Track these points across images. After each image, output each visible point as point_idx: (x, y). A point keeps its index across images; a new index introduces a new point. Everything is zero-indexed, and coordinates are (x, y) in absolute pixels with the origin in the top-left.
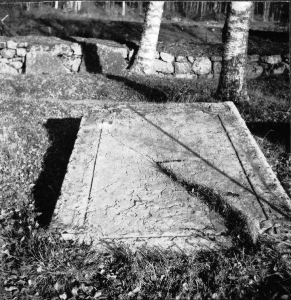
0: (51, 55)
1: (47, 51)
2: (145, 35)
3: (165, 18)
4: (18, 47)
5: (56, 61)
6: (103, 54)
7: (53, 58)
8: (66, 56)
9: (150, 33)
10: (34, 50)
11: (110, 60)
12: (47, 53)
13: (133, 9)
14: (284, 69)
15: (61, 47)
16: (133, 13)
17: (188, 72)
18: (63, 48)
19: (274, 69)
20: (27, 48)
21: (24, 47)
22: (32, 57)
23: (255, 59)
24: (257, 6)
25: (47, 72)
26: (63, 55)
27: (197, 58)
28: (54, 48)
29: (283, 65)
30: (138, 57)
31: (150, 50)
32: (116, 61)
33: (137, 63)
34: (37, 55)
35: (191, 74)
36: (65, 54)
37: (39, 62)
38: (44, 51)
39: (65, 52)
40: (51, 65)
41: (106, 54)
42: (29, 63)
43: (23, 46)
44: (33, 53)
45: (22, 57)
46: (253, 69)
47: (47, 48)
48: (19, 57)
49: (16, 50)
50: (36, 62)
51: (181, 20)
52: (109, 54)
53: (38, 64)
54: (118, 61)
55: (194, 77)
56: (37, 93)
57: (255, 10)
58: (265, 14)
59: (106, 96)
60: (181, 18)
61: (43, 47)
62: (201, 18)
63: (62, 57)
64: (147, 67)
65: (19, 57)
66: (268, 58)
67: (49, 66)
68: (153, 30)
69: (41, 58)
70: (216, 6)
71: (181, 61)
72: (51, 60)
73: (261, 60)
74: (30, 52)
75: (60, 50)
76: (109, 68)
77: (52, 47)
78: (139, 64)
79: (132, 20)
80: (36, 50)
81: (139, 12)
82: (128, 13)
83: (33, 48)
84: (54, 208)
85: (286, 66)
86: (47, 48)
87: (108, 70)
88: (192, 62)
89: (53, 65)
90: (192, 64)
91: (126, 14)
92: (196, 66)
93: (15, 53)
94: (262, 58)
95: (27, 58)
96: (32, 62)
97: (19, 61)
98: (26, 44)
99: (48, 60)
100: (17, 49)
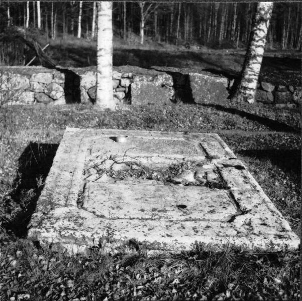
0: (155, 85)
1: (151, 81)
2: (249, 65)
4: (122, 78)
5: (160, 91)
6: (205, 84)
7: (157, 89)
8: (168, 87)
9: (254, 63)
10: (138, 80)
11: (212, 90)
12: (150, 83)
13: (150, 38)
15: (164, 77)
16: (151, 41)
17: (289, 101)
18: (165, 78)
20: (131, 79)
21: (128, 78)
22: (137, 87)
24: (94, 24)
25: (152, 102)
27: (297, 87)
28: (158, 79)
30: (240, 87)
31: (254, 80)
32: (218, 91)
33: (240, 92)
34: (142, 86)
35: (291, 103)
36: (167, 85)
37: (144, 92)
38: (147, 81)
39: (167, 82)
40: (156, 94)
41: (209, 84)
42: (134, 93)
43: (127, 76)
44: (137, 83)
45: (125, 87)
47: (151, 78)
48: (123, 87)
49: (120, 81)
50: (141, 92)
51: (200, 49)
52: (211, 84)
53: (143, 95)
54: (220, 91)
55: (294, 106)
56: (166, 124)
57: (136, 34)
58: (284, 42)
59: (234, 126)
60: (200, 47)
61: (146, 77)
62: (220, 46)
63: (165, 87)
64: (251, 97)
65: (123, 87)
67: (154, 96)
68: (257, 60)
69: (146, 88)
71: (282, 90)
72: (156, 91)
74: (135, 83)
75: (162, 80)
76: (211, 98)
77: (155, 77)
78: (242, 94)
79: (153, 48)
80: (140, 81)
81: (157, 40)
82: (146, 41)
83: (137, 79)
86: (151, 78)
87: (210, 100)
88: (292, 91)
89: (158, 95)
90: (292, 93)
91: (144, 42)
93: (118, 84)
95: (132, 89)
96: (137, 92)
97: (122, 91)
98: (130, 75)
99: (152, 90)
100: (122, 80)
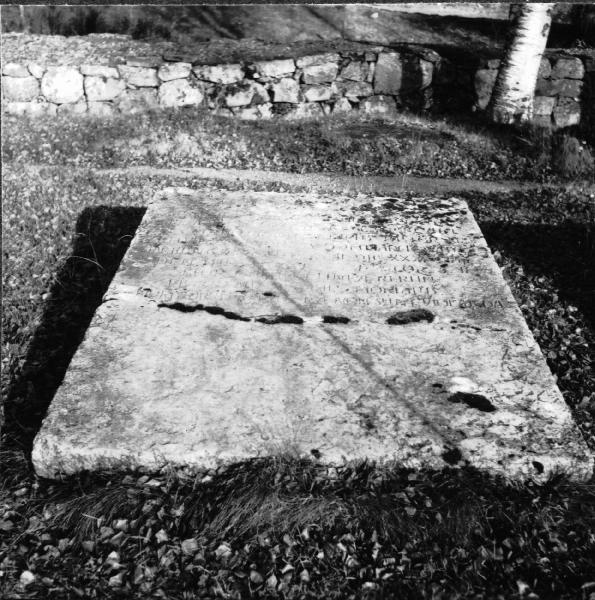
3: (547, 61)
14: (251, 96)
19: (226, 94)
23: (179, 72)
26: (47, 15)
29: (248, 86)
46: (180, 94)
49: (300, 99)
66: (210, 72)
70: (549, 185)
73: (196, 76)
84: (49, 404)
85: (255, 89)
92: (47, 84)
94: (197, 71)
